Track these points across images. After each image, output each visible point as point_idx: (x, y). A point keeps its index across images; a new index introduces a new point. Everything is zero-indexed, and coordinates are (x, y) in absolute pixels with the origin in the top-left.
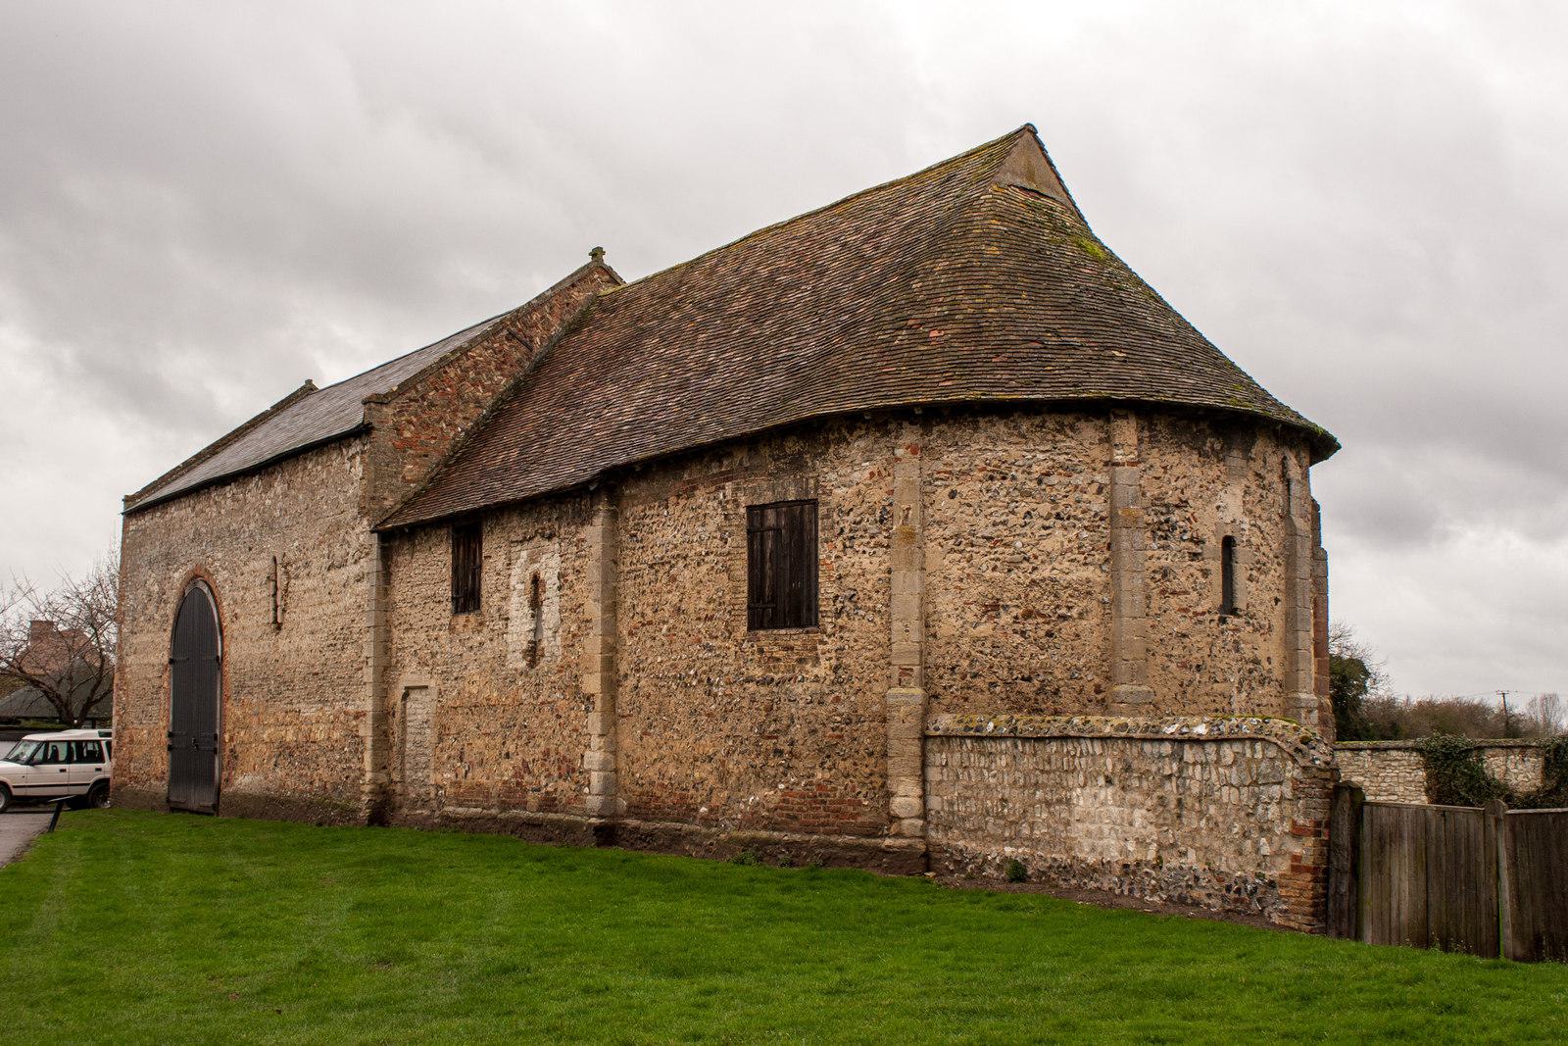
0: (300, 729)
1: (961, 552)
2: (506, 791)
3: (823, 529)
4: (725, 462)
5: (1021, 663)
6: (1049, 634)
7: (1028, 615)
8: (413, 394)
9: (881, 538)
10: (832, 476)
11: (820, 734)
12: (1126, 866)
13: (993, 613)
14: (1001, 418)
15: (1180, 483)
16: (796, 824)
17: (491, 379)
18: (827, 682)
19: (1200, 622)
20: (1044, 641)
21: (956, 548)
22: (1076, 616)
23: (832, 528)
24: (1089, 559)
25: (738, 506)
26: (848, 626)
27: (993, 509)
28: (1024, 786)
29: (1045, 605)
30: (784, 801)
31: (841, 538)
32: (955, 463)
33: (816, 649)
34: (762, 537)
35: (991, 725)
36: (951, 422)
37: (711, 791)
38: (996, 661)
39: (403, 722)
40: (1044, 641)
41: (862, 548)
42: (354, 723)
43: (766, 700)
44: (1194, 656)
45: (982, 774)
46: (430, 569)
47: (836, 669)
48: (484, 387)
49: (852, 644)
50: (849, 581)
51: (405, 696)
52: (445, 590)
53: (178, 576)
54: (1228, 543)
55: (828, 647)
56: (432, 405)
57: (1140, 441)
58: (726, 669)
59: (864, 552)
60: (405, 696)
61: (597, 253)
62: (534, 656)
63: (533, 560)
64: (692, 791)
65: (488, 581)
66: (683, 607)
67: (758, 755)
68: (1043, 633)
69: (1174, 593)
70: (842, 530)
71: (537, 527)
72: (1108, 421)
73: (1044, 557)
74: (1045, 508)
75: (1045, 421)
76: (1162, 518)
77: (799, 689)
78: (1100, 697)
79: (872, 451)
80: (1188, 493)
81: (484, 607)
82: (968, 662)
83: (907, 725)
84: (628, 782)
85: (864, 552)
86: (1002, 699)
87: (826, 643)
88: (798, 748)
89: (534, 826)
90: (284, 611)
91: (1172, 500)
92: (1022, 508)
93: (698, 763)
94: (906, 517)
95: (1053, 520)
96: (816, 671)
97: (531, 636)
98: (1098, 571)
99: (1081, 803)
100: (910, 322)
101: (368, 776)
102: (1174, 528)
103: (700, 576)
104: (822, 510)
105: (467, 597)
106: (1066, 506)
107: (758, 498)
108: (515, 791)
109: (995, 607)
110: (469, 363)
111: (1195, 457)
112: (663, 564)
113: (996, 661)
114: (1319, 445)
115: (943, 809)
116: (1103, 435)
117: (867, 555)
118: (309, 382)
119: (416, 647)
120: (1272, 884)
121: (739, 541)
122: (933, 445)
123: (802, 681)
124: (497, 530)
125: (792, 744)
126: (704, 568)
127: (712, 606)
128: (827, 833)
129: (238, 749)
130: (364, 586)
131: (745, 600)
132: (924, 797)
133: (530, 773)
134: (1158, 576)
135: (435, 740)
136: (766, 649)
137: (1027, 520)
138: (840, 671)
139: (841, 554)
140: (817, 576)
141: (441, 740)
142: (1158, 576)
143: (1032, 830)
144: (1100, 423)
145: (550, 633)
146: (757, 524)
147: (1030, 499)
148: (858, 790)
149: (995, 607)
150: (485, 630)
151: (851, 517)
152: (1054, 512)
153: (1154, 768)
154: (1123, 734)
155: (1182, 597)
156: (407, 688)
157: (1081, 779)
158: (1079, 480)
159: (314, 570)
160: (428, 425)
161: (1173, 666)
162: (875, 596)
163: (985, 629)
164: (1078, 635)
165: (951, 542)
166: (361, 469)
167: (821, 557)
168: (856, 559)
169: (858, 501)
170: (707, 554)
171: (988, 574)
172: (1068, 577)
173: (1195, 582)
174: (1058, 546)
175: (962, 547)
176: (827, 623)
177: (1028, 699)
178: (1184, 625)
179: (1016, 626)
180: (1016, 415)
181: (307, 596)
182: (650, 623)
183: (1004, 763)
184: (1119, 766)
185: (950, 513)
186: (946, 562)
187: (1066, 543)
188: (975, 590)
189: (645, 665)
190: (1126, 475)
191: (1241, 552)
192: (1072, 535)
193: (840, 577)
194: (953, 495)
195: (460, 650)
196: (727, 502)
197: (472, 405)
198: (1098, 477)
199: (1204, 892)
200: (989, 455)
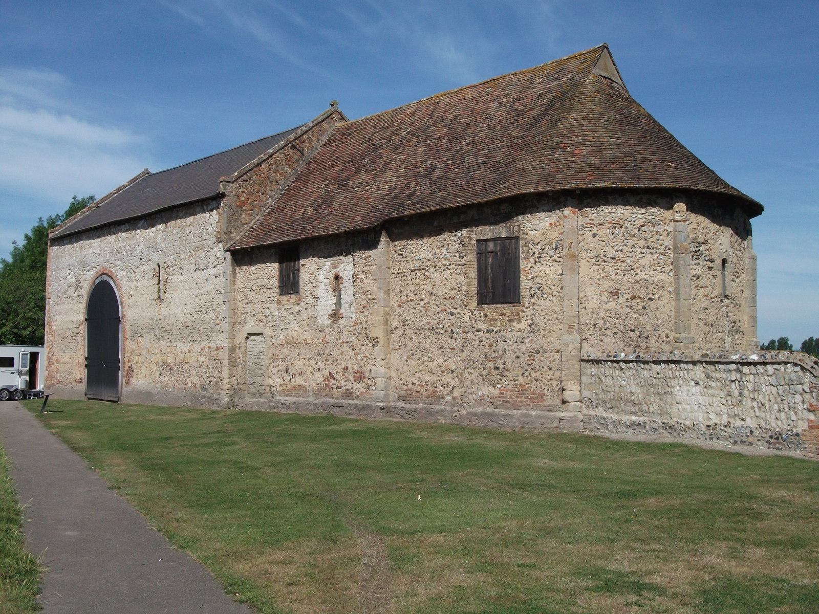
2: (318, 389)
3: (523, 253)
5: (630, 322)
6: (644, 308)
7: (633, 298)
8: (245, 177)
9: (555, 257)
10: (528, 225)
11: (522, 359)
12: (708, 426)
13: (616, 297)
15: (705, 231)
17: (283, 170)
18: (526, 332)
19: (713, 302)
20: (641, 311)
21: (597, 263)
22: (657, 298)
23: (528, 252)
24: (663, 270)
25: (471, 240)
26: (538, 303)
27: (615, 243)
29: (641, 293)
30: (501, 393)
31: (533, 257)
32: (595, 219)
33: (519, 315)
34: (486, 256)
36: (593, 198)
37: (453, 388)
38: (617, 321)
40: (641, 311)
41: (545, 262)
42: (215, 352)
44: (711, 319)
48: (280, 174)
49: (540, 312)
50: (538, 280)
52: (275, 282)
54: (724, 261)
55: (526, 314)
56: (254, 183)
58: (463, 325)
59: (547, 265)
63: (334, 266)
64: (441, 388)
65: (304, 276)
66: (434, 292)
68: (641, 307)
70: (534, 253)
73: (641, 268)
74: (642, 243)
77: (509, 335)
78: (668, 340)
80: (708, 236)
81: (301, 291)
83: (572, 353)
85: (547, 265)
86: (620, 341)
87: (525, 312)
88: (509, 366)
91: (701, 240)
92: (631, 243)
93: (445, 374)
94: (570, 247)
95: (645, 249)
96: (519, 326)
97: (333, 307)
98: (667, 275)
100: (562, 145)
101: (226, 380)
102: (702, 254)
104: (522, 243)
105: (289, 285)
106: (652, 242)
107: (483, 236)
108: (325, 389)
109: (617, 294)
112: (420, 270)
113: (617, 321)
115: (593, 398)
117: (548, 266)
120: (797, 435)
121: (472, 257)
125: (505, 363)
127: (453, 292)
129: (134, 366)
130: (222, 279)
131: (476, 289)
133: (334, 379)
134: (695, 279)
136: (488, 314)
137: (633, 249)
138: (533, 326)
139: (534, 265)
142: (695, 279)
147: (635, 238)
148: (543, 387)
149: (617, 294)
150: (302, 304)
151: (539, 246)
152: (646, 245)
154: (707, 359)
155: (705, 289)
156: (251, 335)
158: (657, 228)
159: (185, 271)
160: (253, 194)
161: (701, 324)
162: (553, 287)
163: (612, 305)
164: (658, 309)
166: (217, 216)
168: (542, 268)
169: (543, 238)
170: (450, 264)
171: (614, 277)
172: (653, 279)
173: (710, 282)
174: (648, 263)
175: (599, 263)
176: (526, 301)
177: (633, 341)
178: (706, 303)
179: (627, 304)
182: (412, 300)
185: (593, 245)
186: (591, 270)
187: (652, 261)
188: (607, 285)
190: (681, 227)
192: (655, 256)
194: (594, 236)
196: (464, 237)
197: (274, 183)
198: (667, 228)
199: (756, 439)
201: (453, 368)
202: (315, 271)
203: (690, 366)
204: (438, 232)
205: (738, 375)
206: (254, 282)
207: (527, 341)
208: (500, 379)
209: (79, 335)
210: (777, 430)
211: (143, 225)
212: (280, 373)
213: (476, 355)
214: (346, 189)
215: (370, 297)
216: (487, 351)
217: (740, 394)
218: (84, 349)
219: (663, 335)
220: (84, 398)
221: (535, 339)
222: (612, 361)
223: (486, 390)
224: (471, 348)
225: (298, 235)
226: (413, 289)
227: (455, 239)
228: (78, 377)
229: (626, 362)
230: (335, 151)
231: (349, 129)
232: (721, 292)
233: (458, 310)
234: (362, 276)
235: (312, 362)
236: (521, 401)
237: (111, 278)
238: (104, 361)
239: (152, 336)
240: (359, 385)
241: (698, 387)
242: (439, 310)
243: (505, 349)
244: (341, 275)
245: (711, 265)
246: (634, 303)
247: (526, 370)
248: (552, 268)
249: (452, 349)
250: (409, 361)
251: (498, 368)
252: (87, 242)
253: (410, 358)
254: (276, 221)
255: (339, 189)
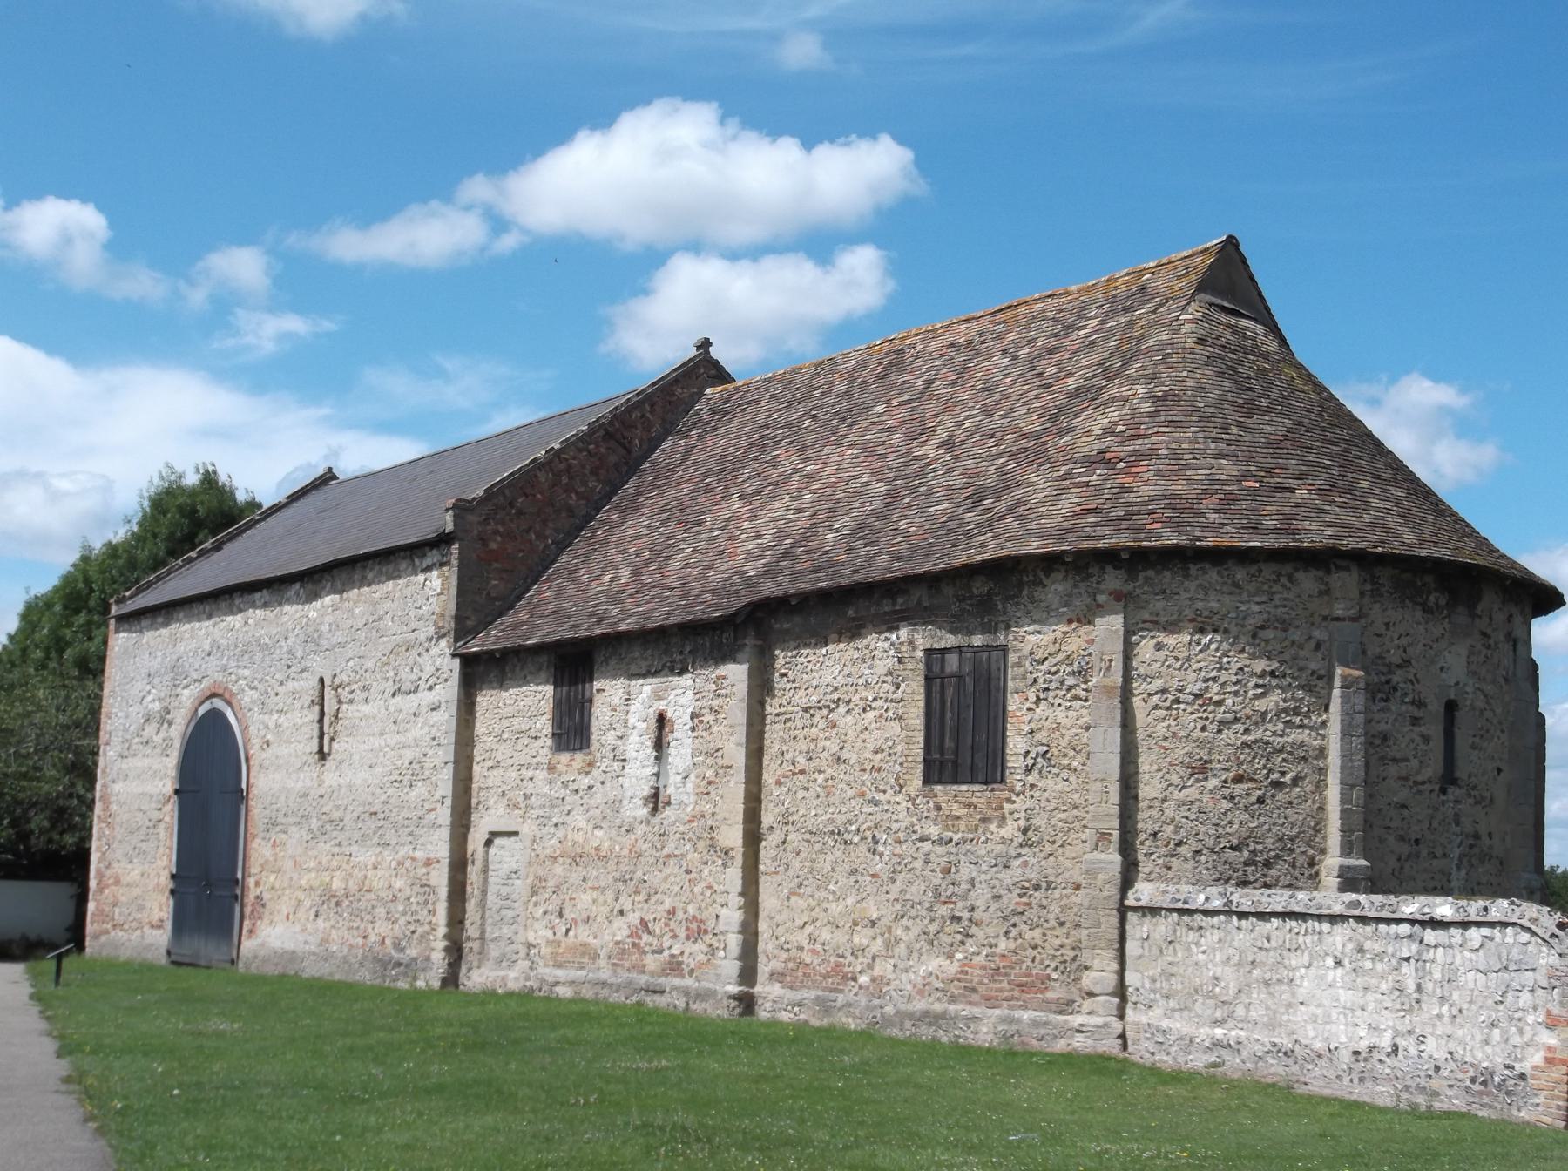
0: (351, 875)
1: (1169, 708)
4: (900, 601)
7: (1239, 779)
11: (1005, 900)
12: (1356, 1053)
14: (1214, 565)
15: (1404, 641)
16: (975, 997)
17: (586, 485)
18: (1015, 844)
19: (1420, 792)
25: (914, 649)
28: (1239, 964)
35: (1202, 897)
38: (1203, 829)
39: (485, 870)
42: (424, 870)
43: (943, 862)
45: (1189, 949)
46: (527, 705)
47: (1025, 831)
51: (488, 843)
52: (544, 725)
53: (188, 696)
54: (1451, 707)
56: (520, 513)
57: (1362, 594)
58: (895, 826)
60: (488, 843)
61: (705, 344)
62: (656, 803)
64: (850, 958)
65: (600, 715)
67: (932, 920)
69: (1394, 760)
70: (1035, 681)
71: (666, 659)
72: (1328, 572)
75: (1260, 571)
76: (1383, 679)
79: (1070, 595)
81: (595, 746)
82: (1172, 827)
83: (1106, 893)
84: (770, 947)
89: (655, 992)
90: (332, 739)
91: (1394, 657)
96: (1003, 832)
99: (1305, 984)
102: (1395, 689)
103: (866, 722)
104: (1012, 658)
105: (572, 730)
110: (562, 466)
111: (1419, 614)
114: (1545, 599)
116: (1323, 587)
118: (330, 469)
119: (504, 787)
120: (1522, 1076)
121: (915, 687)
122: (1138, 591)
123: (986, 842)
124: (613, 662)
126: (871, 715)
127: (879, 756)
128: (1011, 1008)
129: (266, 896)
132: (1121, 973)
134: (1378, 742)
135: (526, 892)
138: (1030, 833)
140: (1004, 729)
141: (534, 893)
143: (1248, 1011)
144: (1320, 573)
145: (679, 778)
146: (936, 669)
151: (1046, 666)
153: (1390, 950)
154: (1357, 912)
155: (1403, 765)
156: (494, 834)
157: (1306, 959)
158: (1296, 635)
159: (373, 694)
165: (1156, 698)
167: (1010, 708)
170: (875, 699)
171: (1196, 734)
176: (1016, 778)
178: (1403, 794)
180: (1230, 563)
181: (363, 723)
182: (802, 772)
183: (1216, 938)
184: (1350, 946)
185: (1156, 666)
188: (1181, 751)
189: (795, 818)
191: (1460, 715)
193: (1032, 732)
195: (562, 793)
200: (1199, 605)
201: (874, 916)
202: (622, 703)
203: (1326, 926)
204: (853, 631)
205: (1415, 947)
206: (506, 723)
207: (1017, 863)
208: (963, 943)
209: (162, 825)
210: (1485, 1064)
211: (297, 594)
212: (548, 917)
213: (915, 892)
214: (699, 533)
215: (720, 762)
216: (938, 882)
217: (1419, 988)
218: (170, 856)
219: (1302, 860)
220: (163, 960)
221: (1032, 861)
222: (1181, 912)
223: (935, 964)
224: (910, 876)
225: (590, 628)
226: (805, 748)
227: (886, 645)
228: (156, 915)
229: (1206, 913)
230: (694, 447)
231: (728, 401)
232: (1440, 771)
233: (887, 797)
234: (708, 718)
235: (610, 896)
236: (1001, 990)
237: (229, 703)
238: (209, 883)
239: (304, 832)
240: (696, 947)
241: (1339, 971)
242: (850, 793)
243: (973, 879)
244: (669, 715)
245: (1417, 713)
246: (1239, 789)
247: (1014, 925)
248: (1070, 713)
249: (873, 876)
250: (793, 899)
251: (959, 919)
252: (187, 626)
253: (794, 894)
254: (558, 596)
255: (686, 531)
